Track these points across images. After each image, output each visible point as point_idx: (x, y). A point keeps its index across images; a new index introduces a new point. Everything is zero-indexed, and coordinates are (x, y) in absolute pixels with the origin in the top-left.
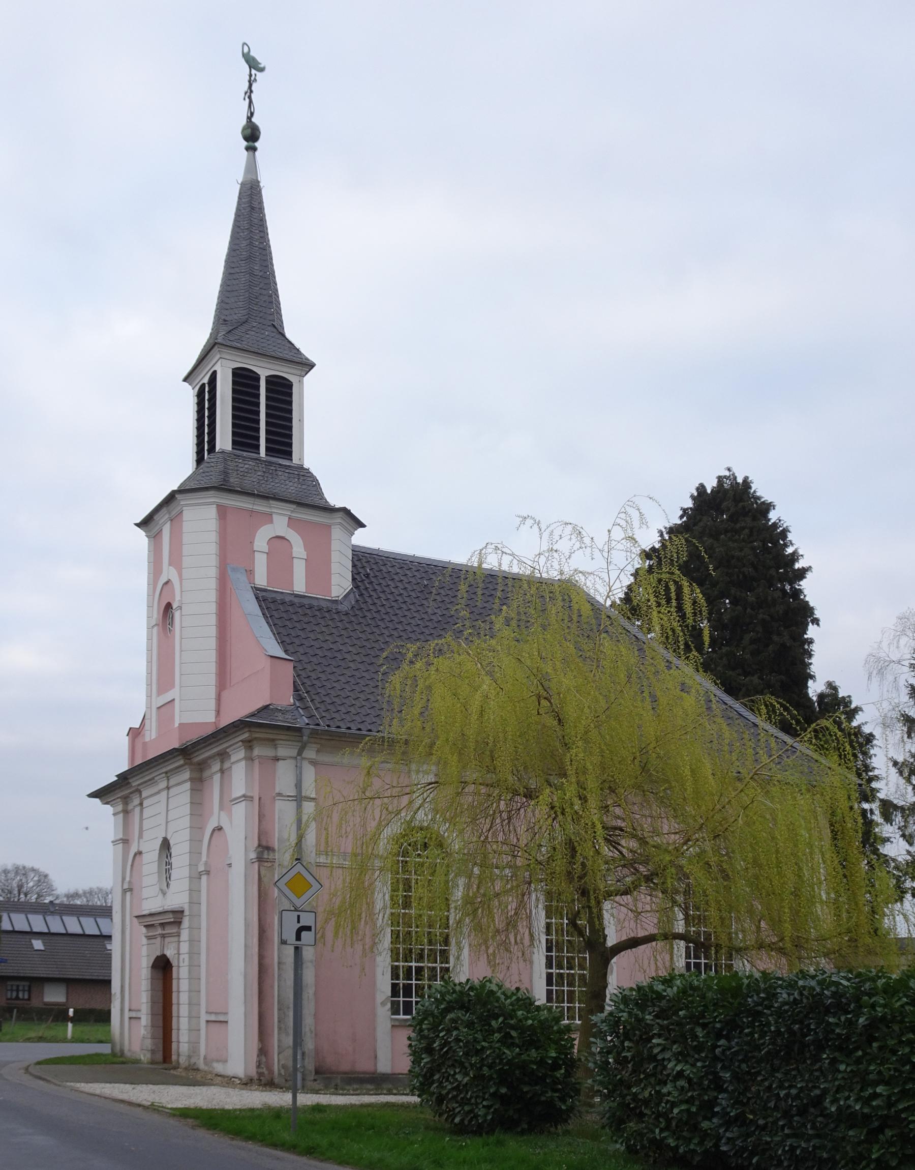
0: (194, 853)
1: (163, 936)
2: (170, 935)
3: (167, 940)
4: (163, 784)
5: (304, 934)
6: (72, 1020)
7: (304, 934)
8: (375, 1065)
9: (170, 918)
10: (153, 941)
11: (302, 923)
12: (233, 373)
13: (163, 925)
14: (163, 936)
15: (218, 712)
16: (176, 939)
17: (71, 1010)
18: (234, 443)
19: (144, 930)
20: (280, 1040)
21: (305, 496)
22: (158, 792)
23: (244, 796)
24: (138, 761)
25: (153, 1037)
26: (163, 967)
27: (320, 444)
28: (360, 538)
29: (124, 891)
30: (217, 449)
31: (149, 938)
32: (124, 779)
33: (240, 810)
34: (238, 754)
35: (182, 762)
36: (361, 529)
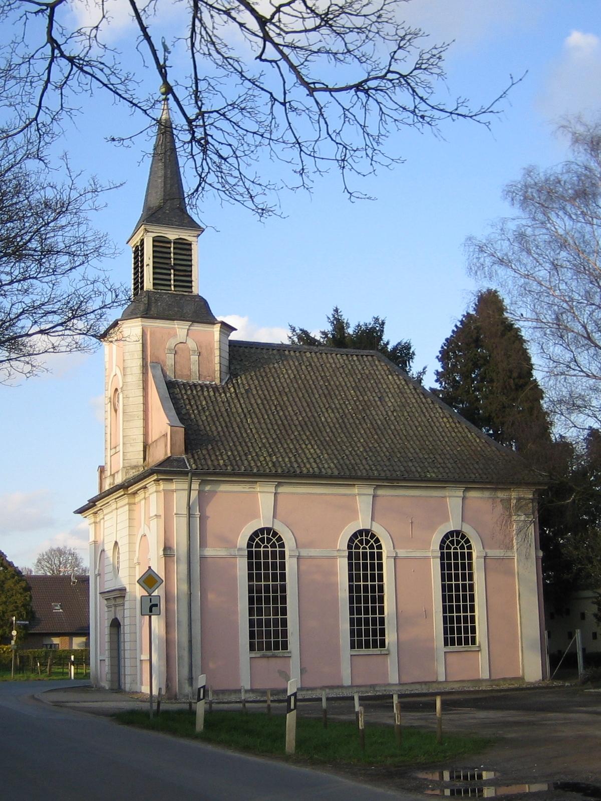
0: (131, 551)
1: (115, 606)
2: (119, 605)
3: (118, 608)
4: (114, 506)
5: (154, 608)
6: (73, 663)
7: (154, 608)
8: (437, 678)
9: (117, 594)
10: (110, 609)
11: (153, 603)
12: (154, 241)
13: (115, 598)
14: (115, 606)
15: (145, 459)
16: (122, 608)
17: (72, 657)
18: (154, 284)
19: (105, 602)
20: (181, 672)
21: (200, 313)
22: (112, 512)
23: (156, 515)
24: (107, 487)
25: (112, 673)
26: (116, 625)
27: (204, 283)
28: (234, 336)
29: (96, 576)
30: (145, 289)
31: (108, 607)
32: (93, 503)
33: (154, 523)
34: (152, 488)
35: (123, 493)
36: (234, 332)
